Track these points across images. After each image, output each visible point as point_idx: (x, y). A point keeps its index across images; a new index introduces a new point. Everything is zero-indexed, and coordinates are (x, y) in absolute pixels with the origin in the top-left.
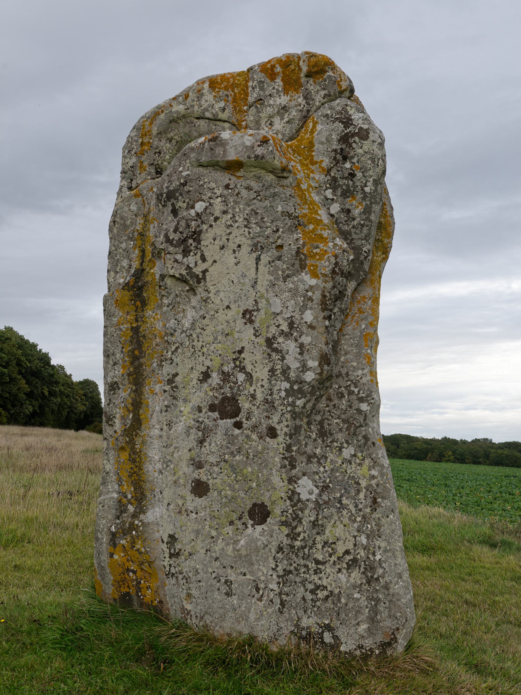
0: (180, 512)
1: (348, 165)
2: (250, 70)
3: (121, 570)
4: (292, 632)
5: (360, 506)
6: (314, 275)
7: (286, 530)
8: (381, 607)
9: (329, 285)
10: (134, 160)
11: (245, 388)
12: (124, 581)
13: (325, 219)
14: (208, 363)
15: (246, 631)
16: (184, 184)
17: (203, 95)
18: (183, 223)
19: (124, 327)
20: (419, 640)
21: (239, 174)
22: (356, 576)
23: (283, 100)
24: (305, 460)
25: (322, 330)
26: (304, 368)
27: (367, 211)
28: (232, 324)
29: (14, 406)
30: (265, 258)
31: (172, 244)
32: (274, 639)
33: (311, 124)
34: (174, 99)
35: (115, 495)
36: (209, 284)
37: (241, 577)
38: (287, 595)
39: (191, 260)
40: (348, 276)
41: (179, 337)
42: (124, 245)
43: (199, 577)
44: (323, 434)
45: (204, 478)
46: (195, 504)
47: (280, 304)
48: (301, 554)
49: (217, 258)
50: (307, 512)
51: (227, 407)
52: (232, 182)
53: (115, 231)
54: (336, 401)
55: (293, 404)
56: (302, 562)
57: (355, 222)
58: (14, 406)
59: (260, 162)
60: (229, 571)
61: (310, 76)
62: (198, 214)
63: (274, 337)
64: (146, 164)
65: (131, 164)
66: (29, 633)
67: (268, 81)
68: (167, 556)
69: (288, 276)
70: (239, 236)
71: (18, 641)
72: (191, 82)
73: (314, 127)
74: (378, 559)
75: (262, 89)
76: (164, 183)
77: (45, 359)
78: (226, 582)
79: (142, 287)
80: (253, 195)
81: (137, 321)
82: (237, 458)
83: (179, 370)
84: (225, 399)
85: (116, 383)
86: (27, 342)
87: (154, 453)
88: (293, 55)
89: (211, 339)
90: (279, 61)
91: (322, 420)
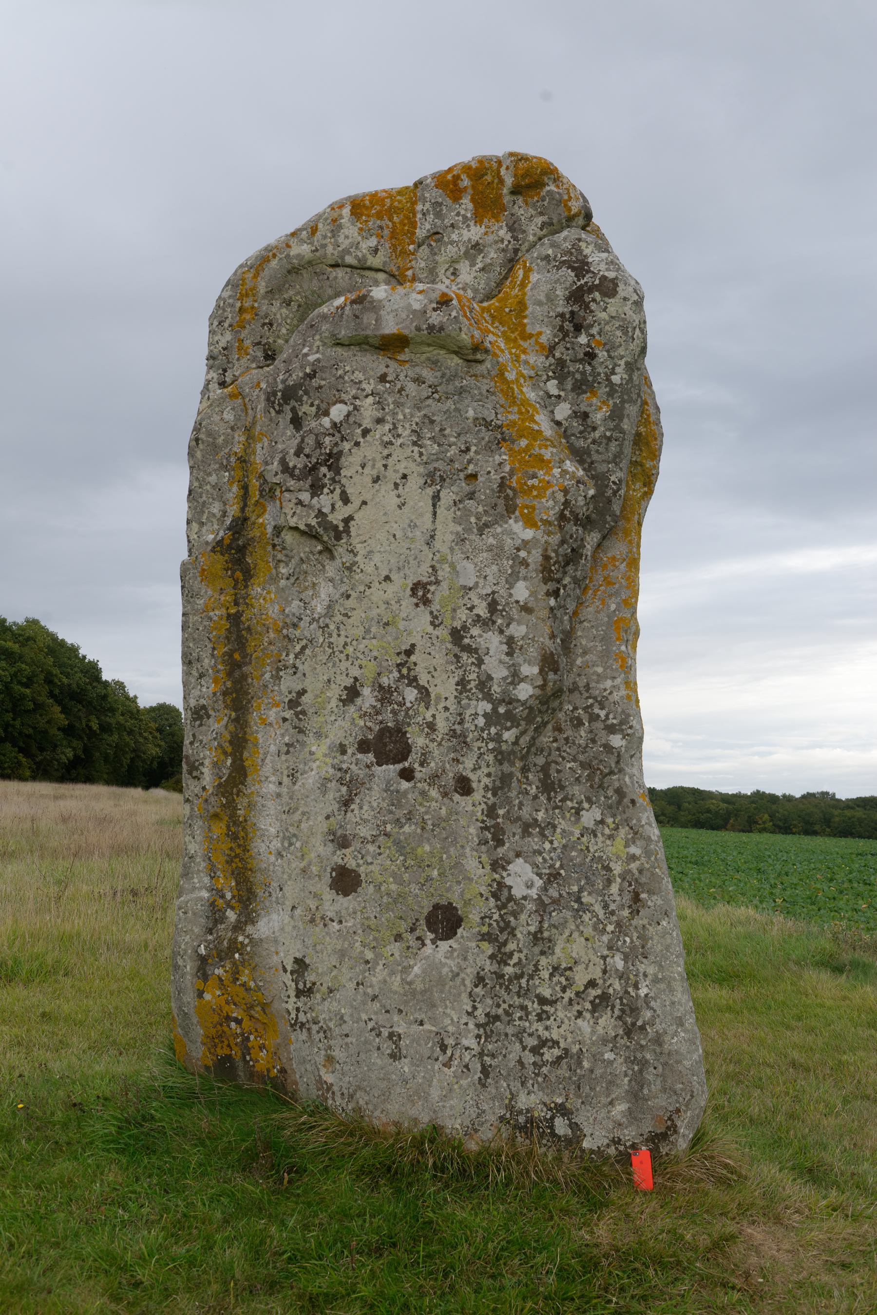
0: (312, 921)
1: (583, 339)
2: (418, 184)
3: (216, 1018)
4: (502, 1118)
5: (613, 907)
6: (530, 522)
7: (488, 949)
8: (650, 1075)
9: (555, 539)
10: (228, 336)
11: (417, 713)
12: (221, 1036)
13: (547, 430)
14: (355, 672)
16: (312, 376)
17: (340, 227)
18: (310, 440)
22: (607, 1023)
23: (475, 233)
24: (520, 830)
25: (544, 613)
26: (516, 678)
27: (617, 414)
28: (395, 607)
29: (42, 749)
30: (447, 496)
31: (292, 475)
32: (472, 1130)
33: (521, 273)
34: (293, 234)
35: (205, 894)
36: (355, 541)
37: (416, 1028)
38: (493, 1056)
39: (324, 501)
40: (587, 523)
41: (306, 629)
42: (213, 479)
43: (346, 1029)
44: (548, 786)
45: (352, 864)
46: (337, 907)
47: (473, 573)
48: (514, 988)
49: (367, 497)
50: (523, 917)
51: (388, 746)
52: (390, 370)
53: (199, 454)
54: (569, 733)
55: (498, 738)
56: (517, 1001)
57: (597, 434)
59: (436, 336)
60: (396, 1018)
61: (517, 191)
62: (334, 425)
63: (464, 628)
64: (247, 343)
65: (223, 344)
67: (449, 201)
68: (292, 993)
69: (486, 525)
70: (404, 459)
71: (47, 1139)
73: (526, 277)
74: (643, 995)
75: (439, 215)
76: (279, 375)
77: (92, 670)
78: (391, 1036)
79: (244, 547)
81: (236, 603)
82: (407, 829)
83: (308, 684)
84: (384, 732)
85: (204, 707)
86: (62, 643)
87: (268, 824)
88: (489, 159)
89: (360, 632)
90: (467, 168)
91: (548, 764)
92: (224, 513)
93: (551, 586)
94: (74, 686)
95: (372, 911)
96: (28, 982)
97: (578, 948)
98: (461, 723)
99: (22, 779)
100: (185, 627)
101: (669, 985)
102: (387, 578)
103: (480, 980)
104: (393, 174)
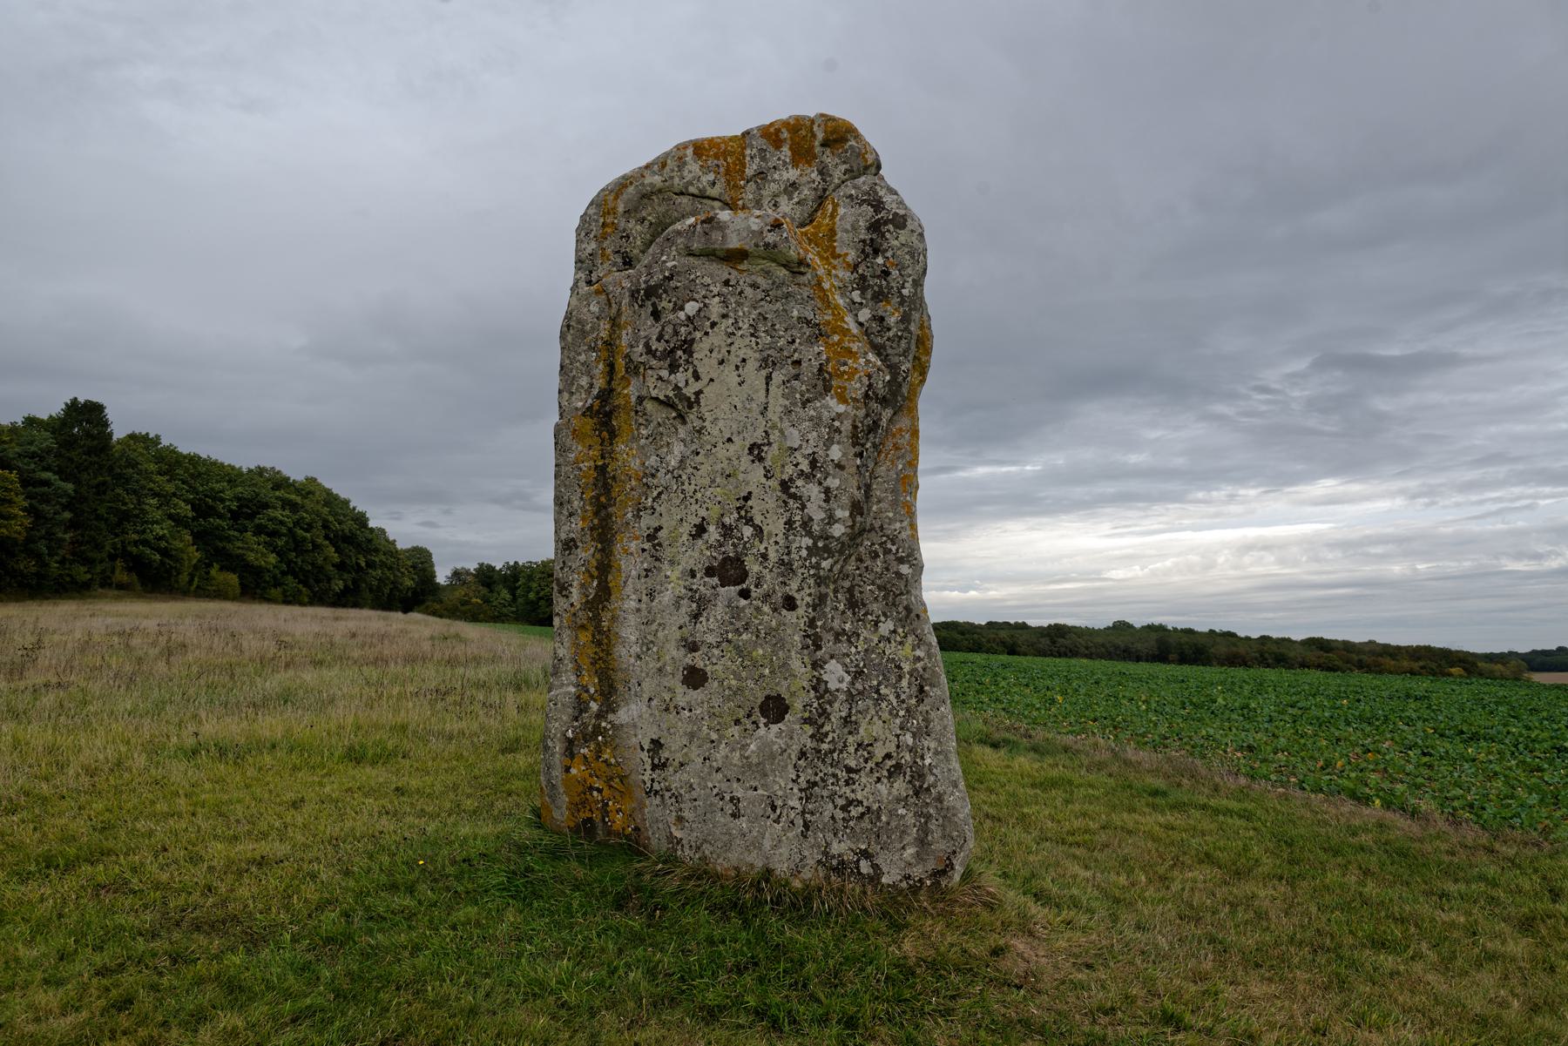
0: (667, 709)
1: (880, 260)
2: (746, 134)
3: (581, 789)
4: (819, 862)
5: (903, 697)
6: (842, 399)
7: (810, 730)
8: (933, 826)
9: (861, 413)
10: (593, 245)
11: (753, 546)
12: (584, 803)
13: (855, 329)
14: (703, 513)
15: (759, 864)
16: (670, 278)
17: (685, 163)
18: (669, 329)
19: (585, 466)
20: (978, 867)
21: (741, 267)
22: (900, 786)
23: (792, 174)
25: (854, 470)
26: (831, 519)
27: (906, 319)
28: (736, 462)
29: (318, 581)
30: (778, 377)
31: (654, 356)
32: (796, 872)
33: (830, 207)
34: (647, 167)
35: (573, 690)
36: (703, 410)
37: (751, 792)
38: (812, 814)
39: (680, 378)
40: (884, 401)
41: (663, 479)
42: (582, 358)
43: (694, 794)
44: (853, 604)
45: (700, 665)
46: (688, 698)
48: (829, 761)
49: (714, 376)
50: (836, 705)
51: (730, 571)
52: (732, 277)
53: (569, 338)
54: (868, 563)
55: (817, 566)
56: (831, 770)
57: (891, 334)
58: (318, 581)
59: (771, 252)
60: (735, 785)
61: (823, 143)
62: (688, 318)
63: (791, 480)
64: (609, 251)
65: (589, 250)
66: (459, 878)
67: (771, 149)
68: (648, 767)
69: (808, 401)
70: (743, 347)
71: (448, 889)
72: (667, 146)
73: (835, 210)
75: (763, 159)
76: (640, 275)
77: (361, 520)
78: (732, 799)
79: (611, 412)
80: (760, 295)
81: (603, 457)
82: (744, 637)
83: (664, 522)
84: (727, 559)
85: (573, 540)
86: (336, 497)
88: (804, 118)
89: (707, 481)
90: (786, 124)
91: (853, 586)
92: (591, 386)
93: (858, 449)
95: (716, 702)
96: (374, 763)
97: (877, 729)
98: (789, 554)
99: (302, 604)
100: (556, 477)
101: (946, 757)
102: (729, 440)
103: (803, 754)
104: (731, 126)
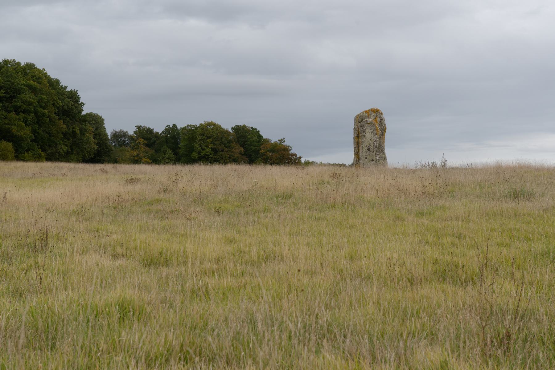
47: (374, 138)
51: (369, 149)
70: (370, 131)
87: (361, 155)
94: (66, 107)
